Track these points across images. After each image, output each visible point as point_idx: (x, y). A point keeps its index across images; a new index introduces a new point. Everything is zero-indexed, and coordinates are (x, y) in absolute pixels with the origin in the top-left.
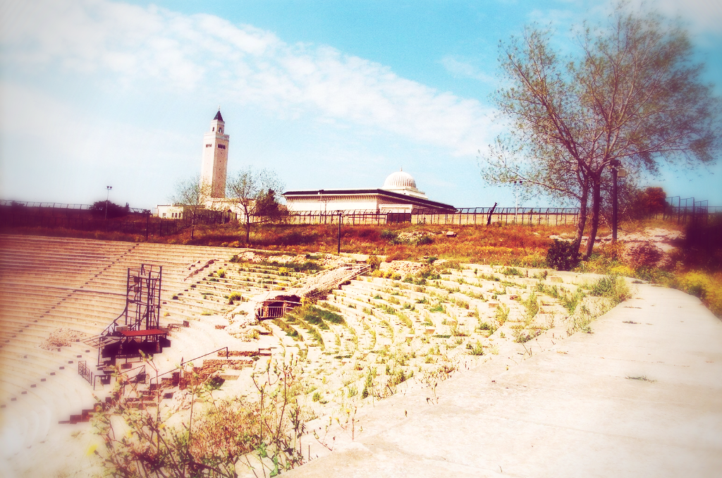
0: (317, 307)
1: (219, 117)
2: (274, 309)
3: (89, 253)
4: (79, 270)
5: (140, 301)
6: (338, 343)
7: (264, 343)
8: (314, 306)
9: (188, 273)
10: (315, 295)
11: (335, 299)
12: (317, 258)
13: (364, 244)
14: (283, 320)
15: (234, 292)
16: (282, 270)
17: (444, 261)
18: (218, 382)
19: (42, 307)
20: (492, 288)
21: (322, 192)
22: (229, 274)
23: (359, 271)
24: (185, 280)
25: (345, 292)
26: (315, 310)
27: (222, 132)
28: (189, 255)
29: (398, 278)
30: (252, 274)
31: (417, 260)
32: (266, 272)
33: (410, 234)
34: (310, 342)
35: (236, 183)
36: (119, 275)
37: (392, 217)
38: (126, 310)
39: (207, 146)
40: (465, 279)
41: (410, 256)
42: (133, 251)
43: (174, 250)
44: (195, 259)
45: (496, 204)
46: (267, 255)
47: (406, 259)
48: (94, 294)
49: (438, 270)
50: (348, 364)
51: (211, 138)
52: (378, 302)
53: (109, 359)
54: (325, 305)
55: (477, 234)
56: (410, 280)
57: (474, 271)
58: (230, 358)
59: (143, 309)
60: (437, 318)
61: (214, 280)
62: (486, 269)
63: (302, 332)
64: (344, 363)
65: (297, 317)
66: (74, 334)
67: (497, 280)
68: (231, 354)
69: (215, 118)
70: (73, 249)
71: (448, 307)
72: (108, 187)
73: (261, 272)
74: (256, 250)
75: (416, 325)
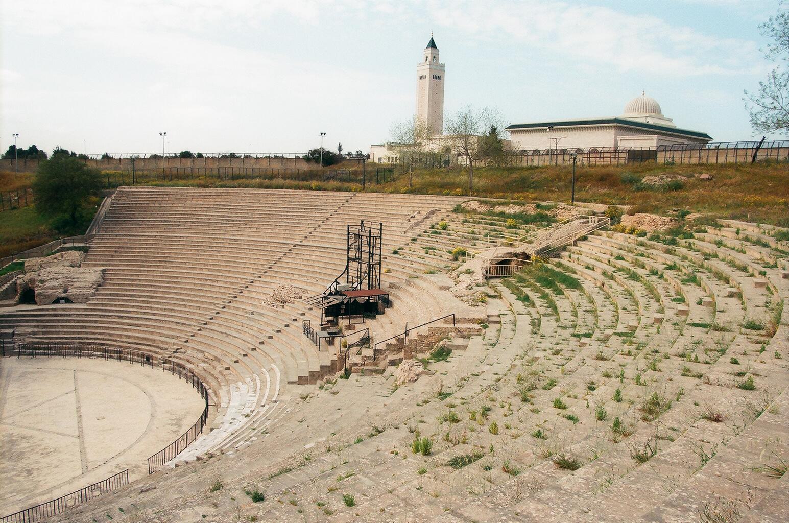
0: (550, 266)
1: (432, 45)
2: (501, 268)
4: (298, 223)
5: (361, 259)
6: (575, 315)
7: (494, 308)
8: (546, 264)
9: (407, 225)
10: (548, 252)
11: (570, 257)
12: (548, 208)
13: (601, 191)
14: (513, 280)
15: (460, 247)
16: (510, 222)
17: (698, 215)
18: (443, 354)
19: (265, 263)
20: (758, 256)
22: (452, 226)
23: (597, 224)
24: (405, 232)
25: (580, 249)
26: (547, 270)
28: (408, 205)
29: (643, 234)
30: (477, 226)
31: (664, 213)
32: (492, 224)
33: (656, 178)
34: (542, 311)
35: (455, 126)
36: (338, 228)
37: (636, 156)
38: (347, 266)
39: (421, 78)
40: (725, 241)
41: (656, 207)
42: (350, 201)
43: (393, 200)
44: (414, 209)
45: (764, 138)
46: (493, 205)
47: (652, 213)
48: (314, 249)
49: (691, 227)
50: (587, 346)
52: (620, 263)
53: (331, 318)
54: (559, 265)
55: (738, 178)
56: (655, 238)
57: (735, 230)
58: (457, 326)
59: (364, 267)
60: (692, 293)
61: (436, 233)
62: (752, 230)
63: (534, 296)
64: (584, 344)
65: (527, 277)
66: (297, 290)
67: (765, 245)
68: (458, 321)
71: (702, 276)
73: (486, 223)
74: (481, 199)
75: (665, 301)
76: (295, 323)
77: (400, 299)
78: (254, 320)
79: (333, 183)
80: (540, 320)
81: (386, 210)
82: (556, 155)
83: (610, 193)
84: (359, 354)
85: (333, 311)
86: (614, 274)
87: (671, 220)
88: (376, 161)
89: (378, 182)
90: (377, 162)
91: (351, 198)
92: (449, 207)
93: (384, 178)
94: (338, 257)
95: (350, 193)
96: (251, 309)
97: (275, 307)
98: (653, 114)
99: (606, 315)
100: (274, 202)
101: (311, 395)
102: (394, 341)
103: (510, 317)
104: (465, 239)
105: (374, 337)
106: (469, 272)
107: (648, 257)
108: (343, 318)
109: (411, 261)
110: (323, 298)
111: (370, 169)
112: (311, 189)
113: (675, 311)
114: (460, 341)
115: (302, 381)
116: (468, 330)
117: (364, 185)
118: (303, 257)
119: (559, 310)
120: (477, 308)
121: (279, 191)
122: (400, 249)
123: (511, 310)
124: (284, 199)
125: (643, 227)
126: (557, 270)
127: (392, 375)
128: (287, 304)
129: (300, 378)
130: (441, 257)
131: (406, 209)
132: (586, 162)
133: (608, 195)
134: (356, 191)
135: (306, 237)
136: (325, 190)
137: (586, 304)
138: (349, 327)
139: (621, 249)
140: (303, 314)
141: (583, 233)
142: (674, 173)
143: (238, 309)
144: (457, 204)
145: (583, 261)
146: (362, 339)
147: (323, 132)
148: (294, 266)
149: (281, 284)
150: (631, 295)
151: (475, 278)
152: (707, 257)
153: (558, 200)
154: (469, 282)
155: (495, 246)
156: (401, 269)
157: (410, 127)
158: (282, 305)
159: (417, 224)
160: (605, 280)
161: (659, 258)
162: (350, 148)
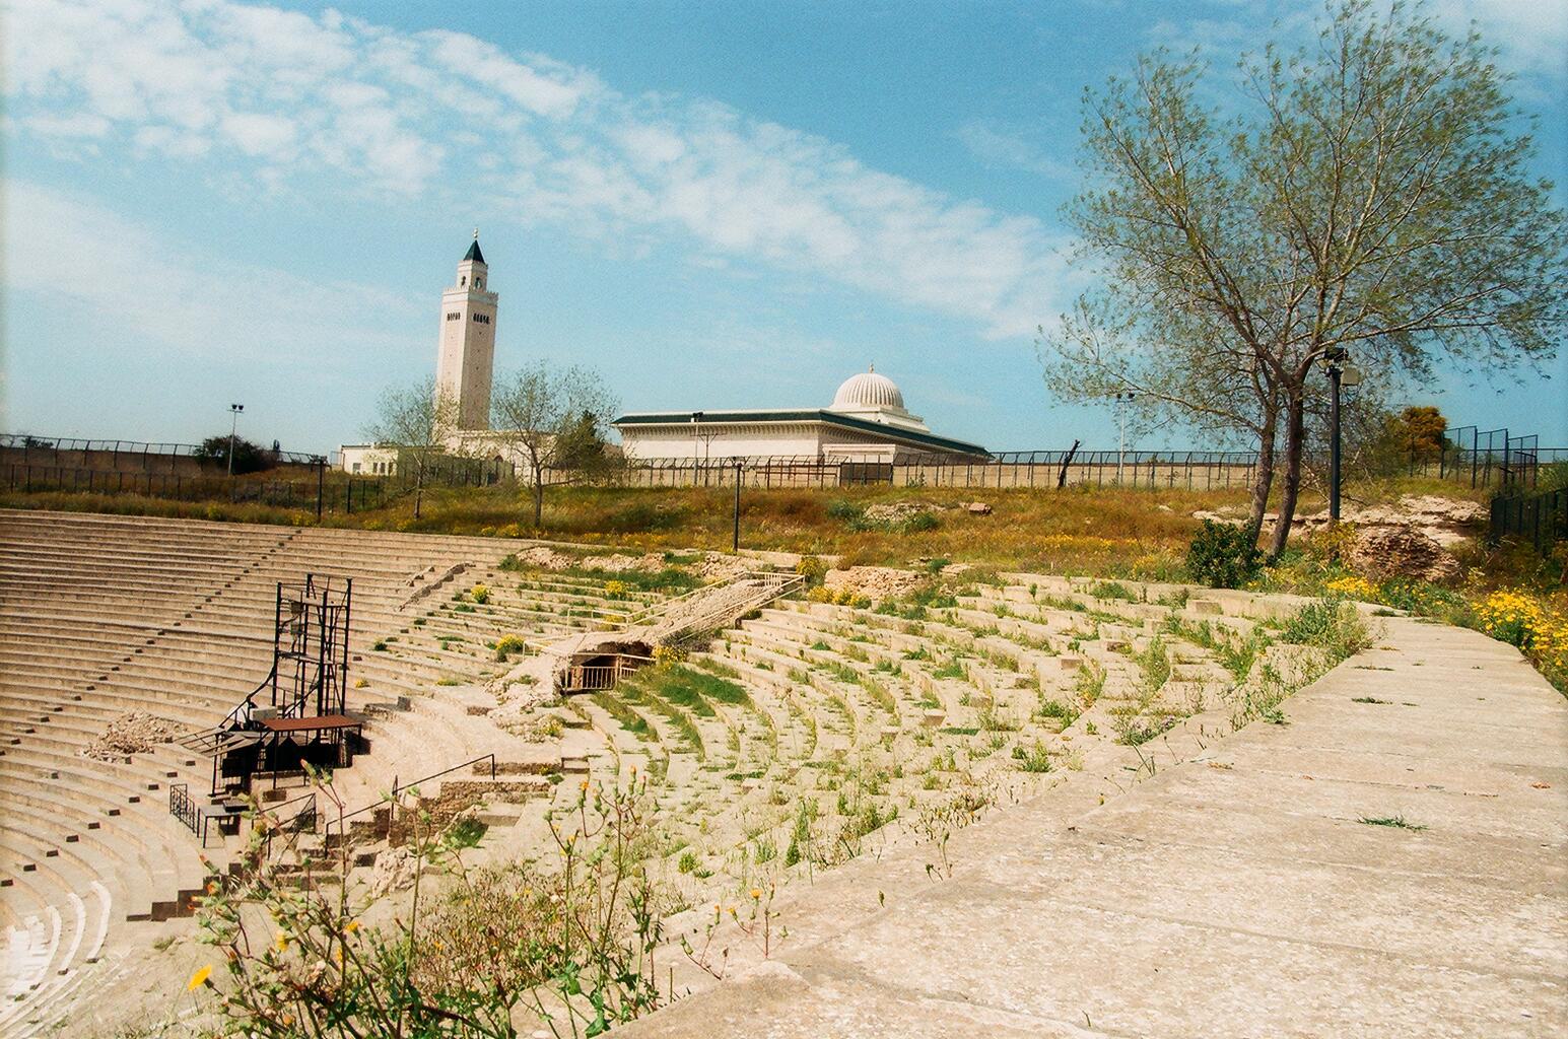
0: (688, 666)
1: (476, 254)
2: (596, 671)
3: (194, 551)
4: (171, 587)
5: (304, 654)
6: (735, 745)
7: (574, 745)
8: (681, 664)
9: (407, 594)
10: (685, 641)
11: (728, 649)
12: (687, 561)
13: (789, 531)
14: (614, 694)
16: (613, 586)
17: (964, 567)
21: (699, 417)
22: (497, 596)
24: (402, 608)
25: (748, 634)
26: (683, 673)
27: (483, 286)
28: (410, 554)
29: (865, 604)
30: (548, 595)
31: (905, 565)
32: (577, 592)
33: (891, 509)
34: (673, 744)
36: (259, 598)
37: (857, 474)
38: (274, 670)
39: (449, 317)
40: (1011, 607)
41: (890, 556)
42: (288, 545)
43: (379, 544)
44: (424, 562)
46: (581, 555)
47: (882, 564)
48: (205, 639)
49: (952, 586)
52: (821, 656)
53: (236, 780)
55: (1035, 510)
56: (888, 608)
59: (312, 673)
61: (465, 609)
62: (1056, 586)
63: (656, 721)
64: (747, 789)
66: (161, 725)
67: (1080, 608)
69: (467, 258)
71: (972, 665)
72: (234, 407)
73: (566, 591)
74: (556, 543)
75: (903, 707)
76: (153, 793)
77: (385, 735)
78: (58, 790)
79: (253, 508)
80: (666, 762)
81: (364, 563)
82: (707, 468)
83: (807, 535)
84: (292, 846)
85: (239, 765)
86: (810, 673)
87: (916, 577)
88: (349, 469)
89: (350, 510)
90: (351, 472)
91: (291, 539)
92: (493, 559)
93: (364, 501)
94: (258, 657)
95: (288, 528)
96: (53, 766)
97: (110, 760)
98: (890, 408)
99: (794, 741)
100: (120, 542)
101: (179, 940)
102: (369, 817)
103: (608, 760)
104: (523, 621)
105: (326, 813)
106: (527, 680)
107: (874, 642)
108: (259, 777)
109: (413, 664)
110: (217, 735)
111: (333, 482)
112: (204, 517)
113: (921, 720)
114: (500, 808)
115: (161, 911)
116: (522, 787)
117: (319, 513)
118: (179, 656)
119: (704, 741)
120: (540, 746)
121: (134, 520)
122: (390, 640)
123: (610, 748)
124: (143, 537)
125: (865, 592)
126: (702, 672)
127: (361, 882)
128: (136, 754)
129: (157, 907)
130: (473, 655)
131: (407, 563)
132: (762, 482)
133: (803, 538)
134: (302, 524)
135: (188, 616)
136: (235, 520)
137: (754, 727)
138: (274, 796)
139: (824, 631)
140: (174, 775)
141: (752, 606)
142: (921, 499)
143: (22, 767)
144: (509, 553)
145: (752, 655)
146: (298, 818)
147: (238, 403)
148: (158, 675)
149: (126, 713)
150: (841, 706)
151: (539, 691)
152: (979, 634)
153: (708, 546)
154: (527, 699)
155: (582, 632)
156: (390, 680)
157: (419, 396)
158: (127, 756)
159: (427, 592)
160: (794, 685)
161: (894, 640)
162: (297, 445)
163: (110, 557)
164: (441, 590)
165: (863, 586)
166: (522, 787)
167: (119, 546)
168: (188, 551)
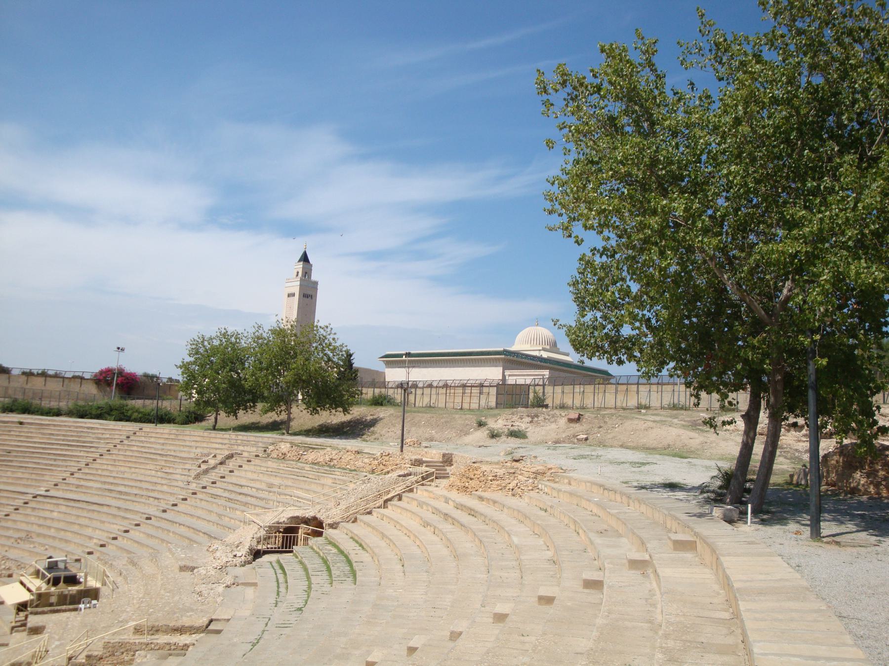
1: (305, 259)
3: (73, 441)
9: (195, 470)
21: (408, 355)
27: (310, 276)
39: (289, 295)
48: (61, 502)
51: (295, 287)
66: (8, 564)
69: (300, 261)
70: (52, 434)
72: (119, 348)
100: (29, 435)
118: (42, 514)
135: (56, 485)
159: (206, 472)
163: (20, 444)
164: (216, 471)
165: (471, 479)
166: (168, 647)
167: (27, 437)
168: (69, 441)
